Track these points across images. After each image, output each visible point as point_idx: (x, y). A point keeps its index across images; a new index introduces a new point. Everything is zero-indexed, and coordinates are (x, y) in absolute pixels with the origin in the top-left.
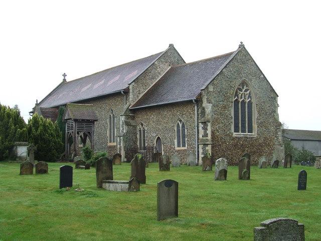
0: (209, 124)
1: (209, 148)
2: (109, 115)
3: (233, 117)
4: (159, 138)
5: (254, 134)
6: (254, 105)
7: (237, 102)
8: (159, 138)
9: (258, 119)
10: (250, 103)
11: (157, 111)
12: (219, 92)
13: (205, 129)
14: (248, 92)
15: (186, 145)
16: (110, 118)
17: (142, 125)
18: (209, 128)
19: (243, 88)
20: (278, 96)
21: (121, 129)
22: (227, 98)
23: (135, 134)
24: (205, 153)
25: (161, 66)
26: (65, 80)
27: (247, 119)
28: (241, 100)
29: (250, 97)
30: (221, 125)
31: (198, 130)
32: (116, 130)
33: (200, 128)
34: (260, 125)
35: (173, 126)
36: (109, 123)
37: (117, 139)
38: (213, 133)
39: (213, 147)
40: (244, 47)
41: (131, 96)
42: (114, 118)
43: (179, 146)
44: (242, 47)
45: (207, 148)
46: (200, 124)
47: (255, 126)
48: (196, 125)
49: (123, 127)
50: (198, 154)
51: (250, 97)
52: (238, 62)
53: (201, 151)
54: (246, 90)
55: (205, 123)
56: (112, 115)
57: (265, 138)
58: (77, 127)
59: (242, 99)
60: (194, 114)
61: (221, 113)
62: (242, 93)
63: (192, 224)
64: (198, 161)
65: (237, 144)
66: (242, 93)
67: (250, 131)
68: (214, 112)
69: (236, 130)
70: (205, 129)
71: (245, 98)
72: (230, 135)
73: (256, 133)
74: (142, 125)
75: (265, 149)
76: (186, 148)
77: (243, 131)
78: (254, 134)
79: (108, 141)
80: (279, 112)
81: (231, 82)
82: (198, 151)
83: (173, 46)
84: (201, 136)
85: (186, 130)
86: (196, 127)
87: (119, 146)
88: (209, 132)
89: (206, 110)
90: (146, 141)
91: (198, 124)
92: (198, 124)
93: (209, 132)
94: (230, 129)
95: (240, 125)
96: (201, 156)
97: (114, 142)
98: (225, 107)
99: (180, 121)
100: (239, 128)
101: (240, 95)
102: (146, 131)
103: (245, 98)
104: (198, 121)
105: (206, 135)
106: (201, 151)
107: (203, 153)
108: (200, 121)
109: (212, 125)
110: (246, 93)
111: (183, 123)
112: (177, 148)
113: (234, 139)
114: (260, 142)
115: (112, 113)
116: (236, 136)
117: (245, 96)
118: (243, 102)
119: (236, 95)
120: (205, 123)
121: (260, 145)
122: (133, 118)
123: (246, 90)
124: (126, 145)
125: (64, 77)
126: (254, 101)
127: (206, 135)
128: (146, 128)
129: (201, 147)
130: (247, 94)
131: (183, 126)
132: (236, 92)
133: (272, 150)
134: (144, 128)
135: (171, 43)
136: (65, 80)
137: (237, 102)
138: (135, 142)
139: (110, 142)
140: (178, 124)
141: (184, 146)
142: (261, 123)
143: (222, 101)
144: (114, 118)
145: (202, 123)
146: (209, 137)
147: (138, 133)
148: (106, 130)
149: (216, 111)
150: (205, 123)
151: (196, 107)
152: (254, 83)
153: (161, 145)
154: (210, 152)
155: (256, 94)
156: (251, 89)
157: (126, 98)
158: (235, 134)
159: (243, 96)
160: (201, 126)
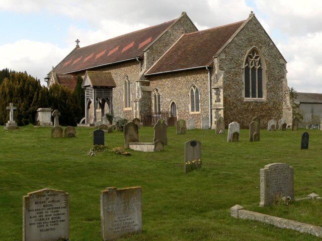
1: (221, 113)
4: (173, 103)
5: (264, 98)
8: (173, 103)
9: (267, 85)
10: (260, 70)
12: (231, 60)
13: (218, 94)
14: (258, 59)
15: (200, 110)
17: (157, 90)
19: (253, 55)
21: (137, 94)
23: (150, 99)
26: (78, 46)
27: (257, 85)
28: (251, 67)
29: (260, 63)
30: (233, 91)
32: (131, 95)
33: (213, 94)
35: (188, 92)
39: (225, 112)
42: (129, 83)
43: (193, 110)
45: (220, 112)
46: (213, 90)
47: (265, 91)
48: (209, 91)
53: (214, 115)
54: (256, 58)
55: (217, 89)
56: (127, 81)
60: (207, 80)
64: (211, 125)
65: (248, 109)
67: (260, 96)
69: (247, 95)
70: (218, 94)
71: (255, 65)
72: (241, 100)
74: (157, 90)
77: (254, 96)
82: (211, 116)
83: (186, 14)
84: (213, 101)
85: (200, 96)
86: (209, 93)
87: (135, 111)
88: (221, 97)
90: (161, 106)
91: (211, 90)
94: (241, 94)
95: (251, 91)
97: (130, 107)
99: (194, 87)
100: (249, 93)
101: (251, 62)
103: (255, 65)
104: (211, 87)
105: (218, 100)
107: (216, 117)
115: (128, 79)
117: (255, 64)
118: (254, 69)
121: (269, 109)
125: (78, 43)
126: (265, 68)
127: (218, 100)
128: (161, 94)
129: (214, 111)
131: (197, 92)
136: (78, 46)
138: (150, 108)
142: (271, 88)
144: (129, 83)
145: (215, 89)
146: (222, 103)
147: (153, 98)
151: (209, 73)
152: (263, 50)
153: (176, 110)
155: (266, 61)
156: (260, 55)
158: (246, 99)
159: (253, 63)
160: (214, 91)
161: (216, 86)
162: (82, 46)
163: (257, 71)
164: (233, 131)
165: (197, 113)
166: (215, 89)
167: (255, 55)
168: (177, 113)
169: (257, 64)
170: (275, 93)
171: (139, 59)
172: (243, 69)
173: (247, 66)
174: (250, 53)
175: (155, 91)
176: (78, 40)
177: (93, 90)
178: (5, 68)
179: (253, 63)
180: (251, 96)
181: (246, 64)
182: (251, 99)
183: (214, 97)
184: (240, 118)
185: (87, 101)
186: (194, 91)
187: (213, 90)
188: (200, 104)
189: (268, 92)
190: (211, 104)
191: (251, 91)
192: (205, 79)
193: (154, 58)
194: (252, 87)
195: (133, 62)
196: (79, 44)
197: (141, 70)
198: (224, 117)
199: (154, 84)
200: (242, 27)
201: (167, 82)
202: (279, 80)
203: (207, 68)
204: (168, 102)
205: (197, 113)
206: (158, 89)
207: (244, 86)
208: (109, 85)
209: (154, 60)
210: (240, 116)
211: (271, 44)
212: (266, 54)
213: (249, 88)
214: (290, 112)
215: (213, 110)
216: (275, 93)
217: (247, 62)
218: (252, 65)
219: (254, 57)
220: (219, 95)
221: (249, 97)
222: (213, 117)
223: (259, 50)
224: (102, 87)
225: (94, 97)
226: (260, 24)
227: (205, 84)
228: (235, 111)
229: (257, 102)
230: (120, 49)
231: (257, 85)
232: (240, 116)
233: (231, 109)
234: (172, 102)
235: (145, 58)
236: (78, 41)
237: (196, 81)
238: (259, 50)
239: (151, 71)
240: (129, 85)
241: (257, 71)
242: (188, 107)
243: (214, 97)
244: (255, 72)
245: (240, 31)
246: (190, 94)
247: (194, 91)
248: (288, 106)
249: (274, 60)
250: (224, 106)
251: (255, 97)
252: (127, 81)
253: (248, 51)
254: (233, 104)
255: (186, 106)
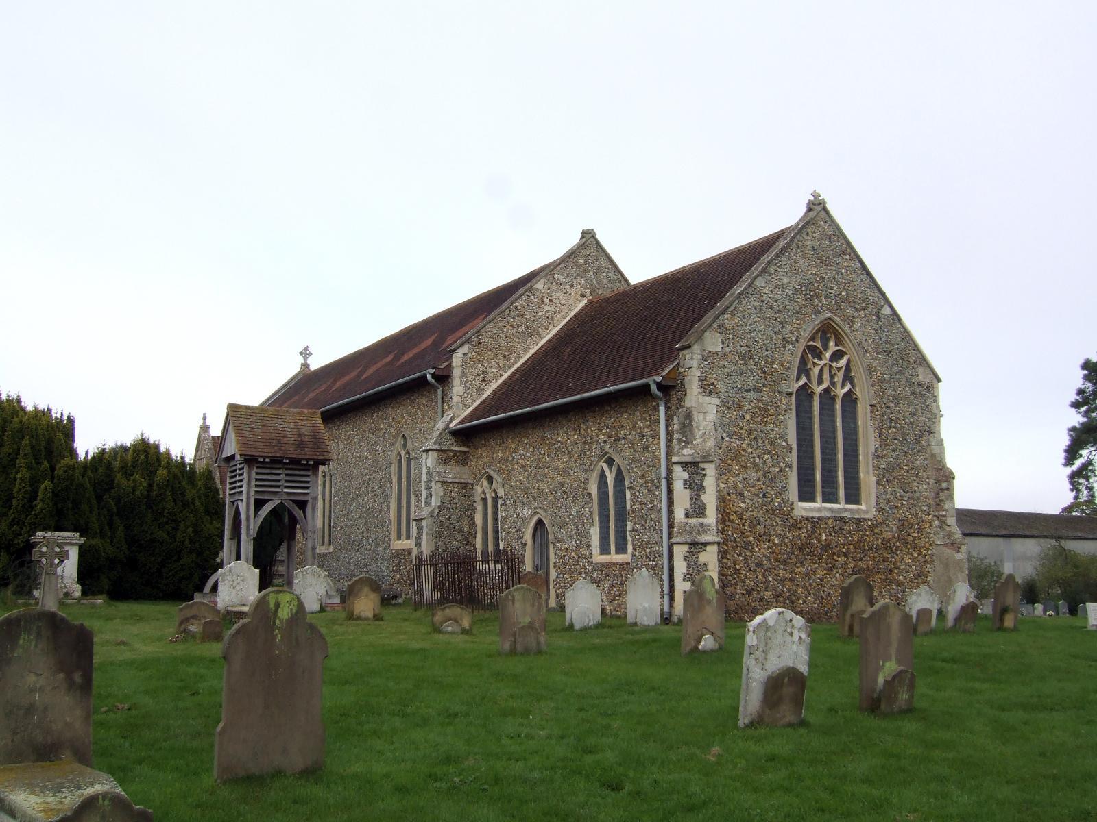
0: (710, 470)
1: (710, 557)
2: (395, 453)
3: (794, 446)
4: (540, 523)
6: (863, 409)
7: (804, 394)
10: (850, 401)
11: (535, 435)
12: (743, 357)
13: (695, 487)
14: (843, 362)
16: (400, 461)
17: (490, 479)
18: (710, 482)
19: (826, 348)
20: (939, 381)
21: (425, 493)
22: (771, 379)
23: (471, 510)
24: (695, 573)
25: (555, 296)
26: (305, 366)
27: (840, 456)
28: (818, 390)
29: (848, 378)
30: (753, 475)
31: (670, 492)
32: (412, 496)
33: (678, 486)
34: (886, 476)
35: (586, 482)
36: (395, 479)
37: (414, 530)
38: (723, 502)
39: (723, 555)
40: (825, 209)
41: (457, 387)
42: (409, 460)
43: (605, 550)
44: (819, 208)
45: (703, 557)
46: (677, 469)
47: (868, 479)
48: (663, 474)
49: (429, 488)
50: (671, 579)
51: (848, 378)
52: (805, 256)
53: (680, 567)
54: (837, 356)
55: (693, 467)
56: (403, 453)
57: (903, 523)
58: (253, 483)
59: (824, 386)
60: (655, 435)
61: (750, 432)
62: (822, 363)
63: (666, 609)
64: (671, 606)
65: (809, 543)
66: (822, 363)
67: (853, 496)
68: (721, 425)
69: (806, 494)
70: (695, 487)
71: (833, 383)
72: (783, 512)
73: (874, 503)
74: (490, 479)
75: (902, 560)
76: (626, 557)
77: (830, 497)
78: (866, 508)
79: (394, 536)
80: (943, 436)
81: (783, 324)
82: (671, 570)
83: (594, 237)
84: (679, 514)
85: (628, 493)
86: (664, 483)
88: (710, 498)
89: (697, 417)
90: (502, 535)
91: (671, 547)
92: (670, 471)
93: (710, 498)
94: (784, 489)
95: (818, 477)
96: (682, 586)
97: (408, 537)
98: (765, 412)
99: (610, 462)
100: (814, 487)
101: (816, 370)
102: (500, 502)
103: (833, 383)
104: (668, 461)
105: (698, 509)
106: (680, 567)
107: (688, 577)
108: (675, 459)
109: (722, 472)
110: (834, 365)
111: (619, 469)
112: (599, 558)
113: (796, 525)
114: (887, 535)
116: (804, 514)
117: (832, 377)
119: (803, 370)
120: (693, 467)
121: (887, 545)
122: (463, 460)
123: (837, 356)
124: (437, 548)
125: (305, 359)
126: (864, 394)
127: (698, 509)
128: (501, 492)
129: (680, 551)
130: (839, 369)
131: (619, 479)
132: (803, 361)
133: (926, 562)
134: (495, 491)
135: (586, 229)
136: (305, 366)
137: (804, 394)
138: (468, 539)
139: (399, 538)
140: (603, 471)
141: (621, 549)
142: (890, 469)
143: (756, 389)
145: (684, 465)
146: (711, 517)
147: (480, 507)
148: (386, 498)
149: (733, 423)
150: (695, 464)
151: (662, 410)
152: (859, 331)
153: (548, 547)
154: (713, 573)
155: (870, 370)
156: (852, 353)
157: (444, 395)
158: (803, 508)
159: (826, 376)
160: (680, 475)
161: (687, 453)
162: (315, 364)
163: (838, 406)
164: (775, 664)
165: (620, 558)
166: (684, 465)
167: (832, 346)
168: (552, 561)
169: (839, 378)
170: (904, 485)
171: (433, 375)
172: (790, 394)
173: (805, 387)
174: (813, 339)
175: (485, 483)
176: (306, 348)
177: (245, 471)
178: (60, 408)
179: (826, 376)
180: (819, 498)
181: (798, 379)
182: (820, 510)
183: (682, 498)
184: (782, 580)
185: (230, 507)
186: (610, 477)
187: (677, 469)
188: (629, 526)
189: (878, 482)
190: (671, 525)
191: (818, 477)
192: (647, 431)
193: (485, 372)
194: (828, 467)
195: (418, 386)
196: (309, 361)
197: (443, 413)
198: (722, 574)
199: (488, 456)
200: (781, 244)
201: (521, 452)
202: (917, 440)
203: (653, 387)
204: (524, 519)
205: (620, 558)
206: (492, 473)
207: (793, 458)
208: (309, 454)
209: (484, 381)
210: (782, 573)
211: (886, 311)
212: (869, 345)
213: (813, 469)
214: (958, 556)
215: (677, 549)
216: (904, 485)
217: (803, 370)
218: (820, 382)
219: (828, 355)
220: (701, 488)
221: (813, 500)
222: (678, 577)
223: (847, 329)
224: (276, 462)
225: (248, 498)
226: (845, 238)
227: (646, 448)
228: (761, 552)
229: (842, 519)
230: (397, 358)
231: (840, 456)
232: (782, 573)
233: (748, 546)
234: (535, 519)
235: (457, 372)
236: (306, 353)
237: (617, 440)
238: (847, 329)
239: (471, 417)
240: (409, 465)
241: (838, 406)
242: (588, 537)
243: (682, 498)
244: (833, 410)
245: (777, 256)
246: (594, 489)
247: (610, 477)
248: (949, 535)
249: (895, 369)
250: (721, 532)
251: (836, 501)
252: (403, 453)
253: (807, 332)
254: (752, 526)
255: (583, 535)
